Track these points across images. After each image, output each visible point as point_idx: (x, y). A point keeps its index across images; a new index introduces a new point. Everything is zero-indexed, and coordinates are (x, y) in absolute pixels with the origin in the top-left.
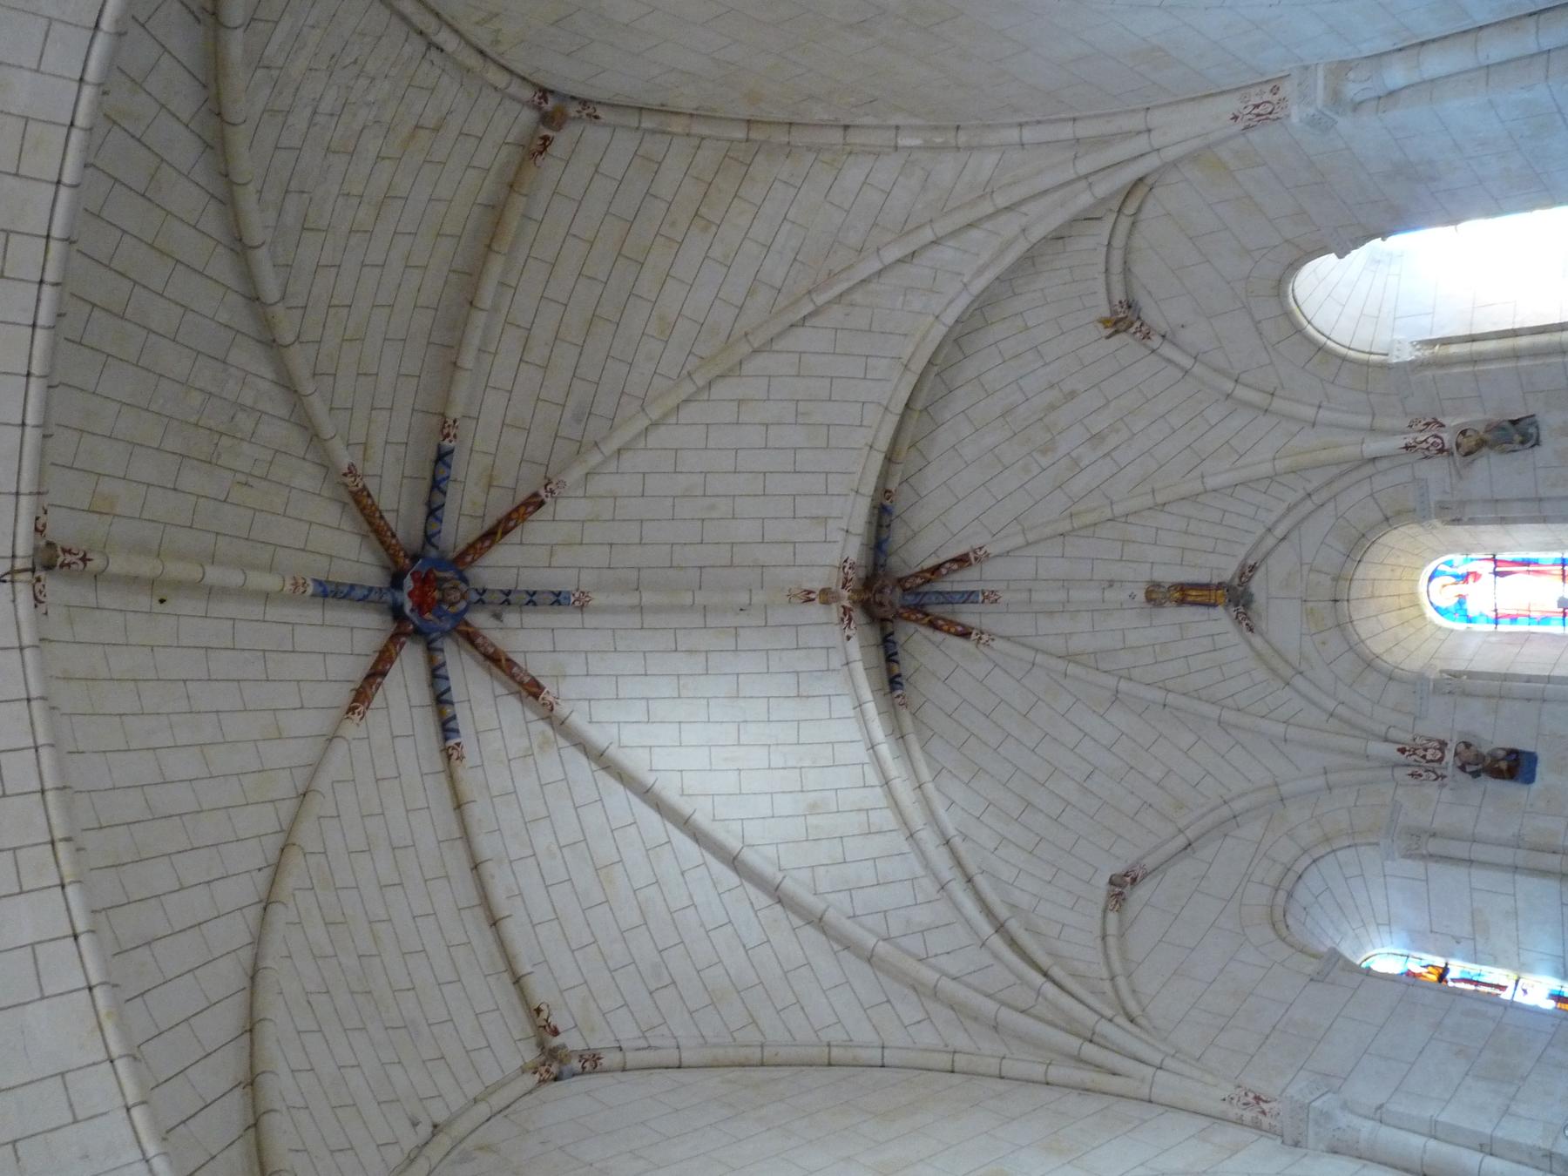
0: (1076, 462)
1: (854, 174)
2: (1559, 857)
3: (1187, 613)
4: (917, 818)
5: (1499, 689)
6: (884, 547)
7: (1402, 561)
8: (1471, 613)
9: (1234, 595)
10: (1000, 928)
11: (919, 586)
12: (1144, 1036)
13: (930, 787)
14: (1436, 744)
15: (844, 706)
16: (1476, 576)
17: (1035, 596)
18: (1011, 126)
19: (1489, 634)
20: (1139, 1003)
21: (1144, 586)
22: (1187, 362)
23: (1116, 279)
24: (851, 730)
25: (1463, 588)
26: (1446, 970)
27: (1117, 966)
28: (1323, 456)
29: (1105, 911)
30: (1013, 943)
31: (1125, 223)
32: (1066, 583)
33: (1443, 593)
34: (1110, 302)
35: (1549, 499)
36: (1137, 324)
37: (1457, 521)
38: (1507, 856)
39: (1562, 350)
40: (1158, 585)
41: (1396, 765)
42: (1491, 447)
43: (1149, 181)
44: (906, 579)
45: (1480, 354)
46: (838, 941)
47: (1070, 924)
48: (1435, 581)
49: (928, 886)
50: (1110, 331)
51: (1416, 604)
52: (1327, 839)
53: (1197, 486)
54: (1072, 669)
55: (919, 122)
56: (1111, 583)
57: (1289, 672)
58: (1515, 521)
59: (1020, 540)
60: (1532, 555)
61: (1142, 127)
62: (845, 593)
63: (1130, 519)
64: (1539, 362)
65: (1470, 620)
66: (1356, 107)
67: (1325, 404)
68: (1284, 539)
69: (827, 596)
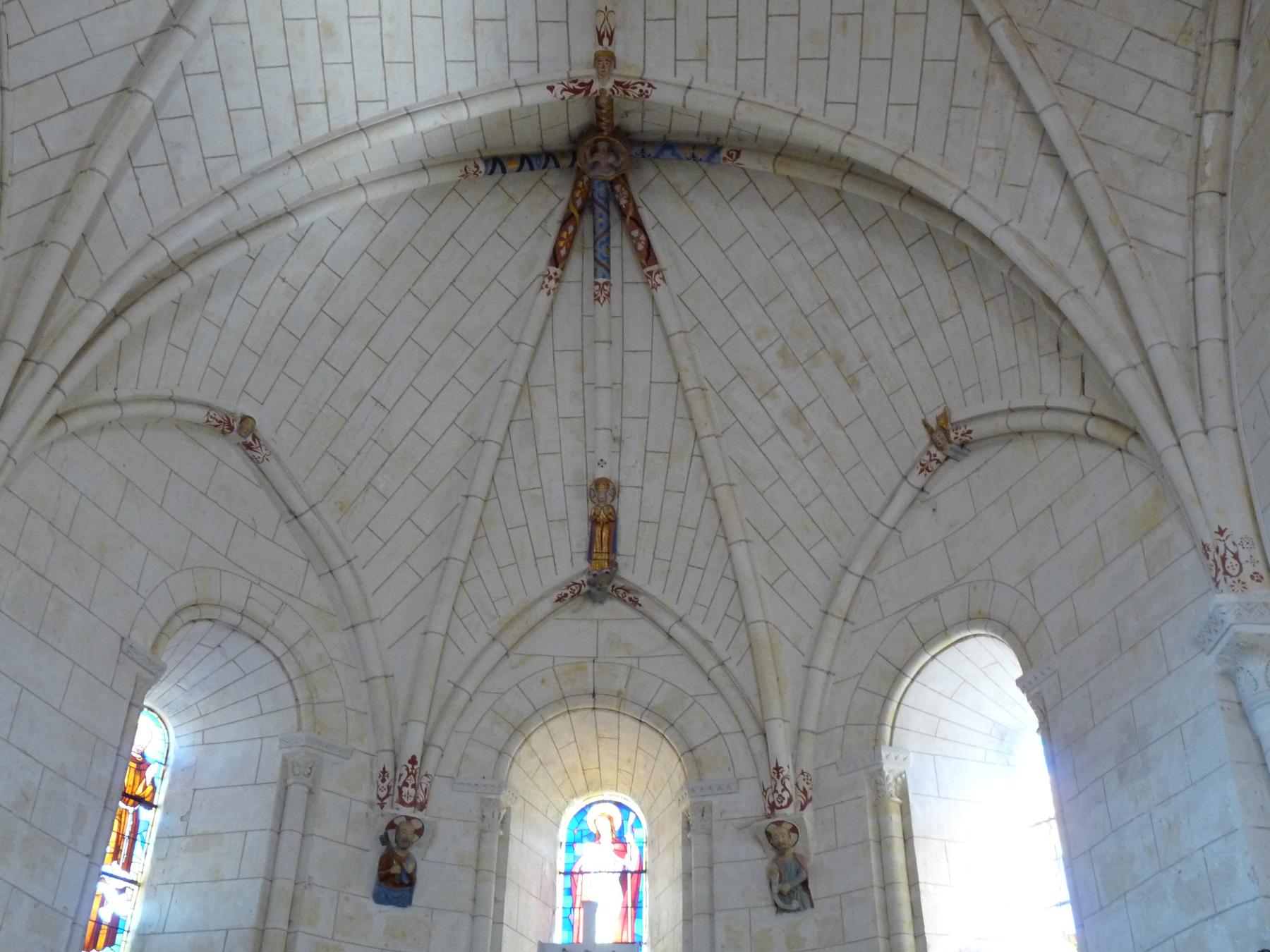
0: (770, 393)
1: (1169, 64)
2: (284, 926)
3: (581, 528)
4: (319, 171)
5: (488, 868)
6: (667, 154)
7: (641, 772)
8: (578, 846)
9: (601, 582)
10: (177, 267)
11: (617, 203)
12: (37, 425)
13: (360, 198)
14: (421, 799)
15: (463, 80)
16: (622, 852)
17: (602, 349)
18: (1222, 262)
19: (553, 865)
20: (87, 430)
21: (614, 478)
22: (890, 517)
23: (1000, 424)
24: (431, 88)
25: (607, 837)
26: (150, 805)
27: (131, 410)
28: (770, 677)
29: (207, 406)
30: (156, 280)
31: (1075, 423)
32: (619, 387)
33: (601, 819)
34: (971, 419)
35: (712, 923)
36: (940, 456)
37: (687, 826)
38: (286, 869)
39: (892, 934)
40: (615, 493)
41: (396, 755)
42: (775, 860)
43: (1133, 445)
44: (626, 186)
45: (889, 847)
46: (150, 50)
47: (186, 359)
48: (616, 809)
49: (229, 175)
50: (933, 424)
51: (588, 788)
52: (305, 674)
53: (736, 534)
54: (513, 389)
55: (1235, 144)
56: (618, 440)
57: (509, 638)
58: (687, 888)
59: (672, 327)
60: (645, 912)
61: (1211, 423)
62: (609, 85)
63: (697, 460)
64: (878, 911)
65: (571, 845)
66: (1229, 676)
67: (833, 679)
68: (670, 637)
69: (605, 61)
